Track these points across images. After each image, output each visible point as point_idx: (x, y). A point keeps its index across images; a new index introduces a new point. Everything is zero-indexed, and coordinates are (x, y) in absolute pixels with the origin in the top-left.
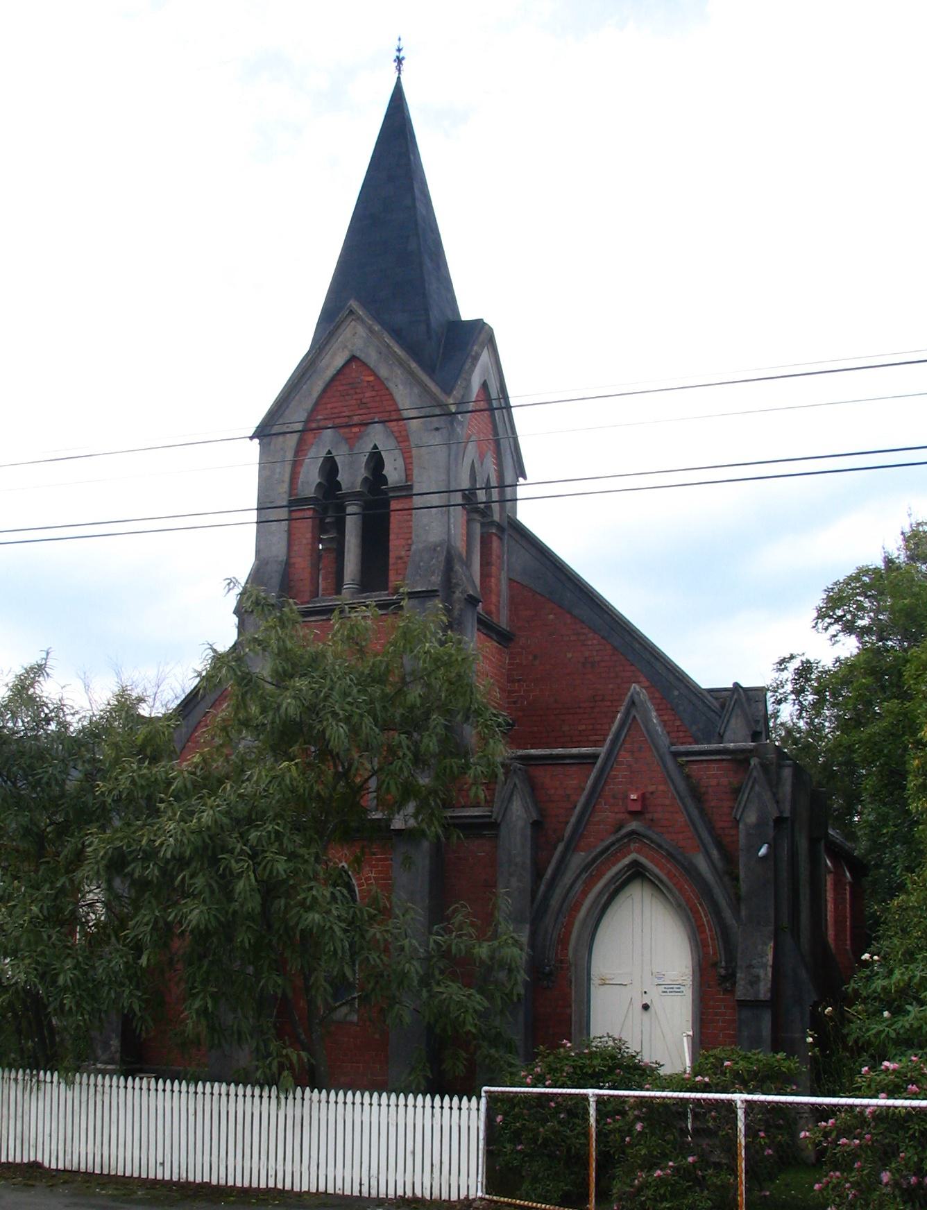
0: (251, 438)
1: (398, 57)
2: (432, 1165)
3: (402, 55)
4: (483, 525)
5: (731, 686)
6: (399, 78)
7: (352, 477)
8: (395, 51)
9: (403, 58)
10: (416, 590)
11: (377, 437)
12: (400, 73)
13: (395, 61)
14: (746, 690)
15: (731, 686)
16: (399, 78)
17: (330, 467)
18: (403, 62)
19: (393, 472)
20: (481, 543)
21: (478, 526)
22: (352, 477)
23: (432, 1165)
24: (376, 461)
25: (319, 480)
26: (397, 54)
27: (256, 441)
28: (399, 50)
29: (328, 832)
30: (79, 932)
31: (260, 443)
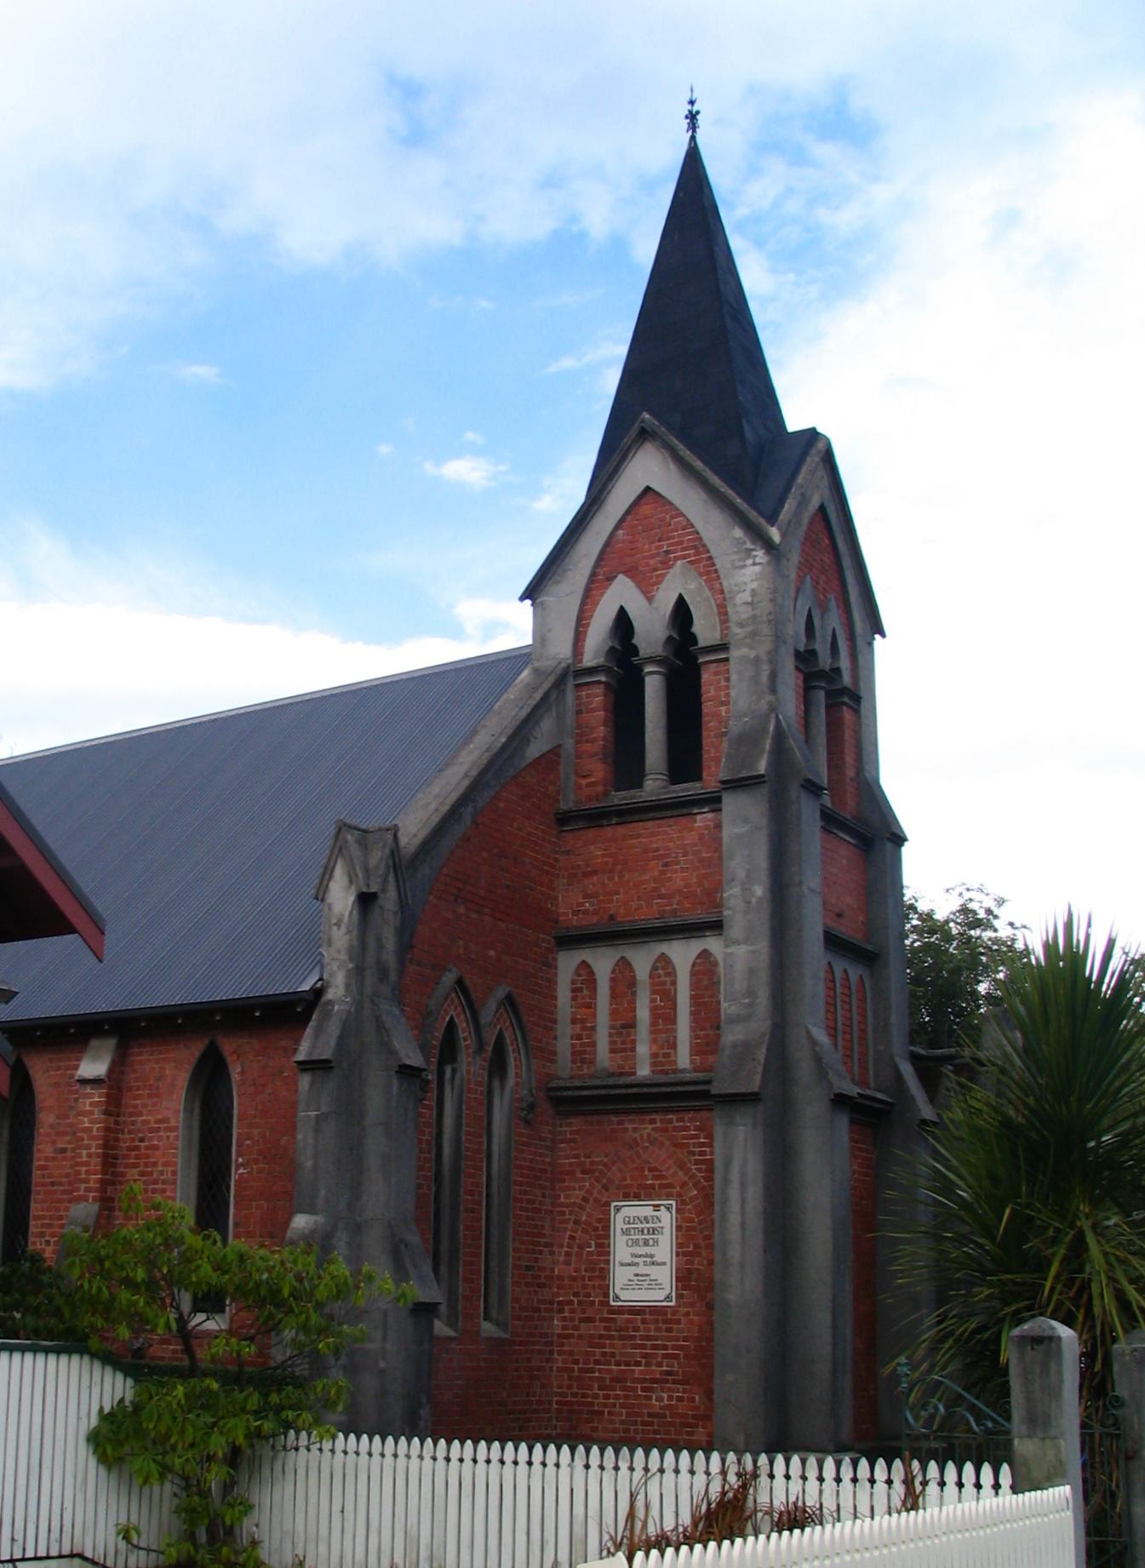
0: (522, 599)
1: (690, 112)
2: (49, 1531)
3: (695, 109)
4: (828, 694)
5: (794, 422)
6: (693, 138)
7: (651, 629)
8: (686, 104)
9: (698, 112)
10: (741, 776)
11: (677, 583)
12: (694, 131)
13: (687, 117)
14: (818, 433)
15: (794, 422)
16: (693, 138)
17: (623, 623)
18: (698, 117)
19: (705, 630)
20: (828, 725)
21: (822, 694)
22: (651, 629)
23: (49, 1531)
24: (682, 613)
25: (610, 644)
26: (690, 107)
27: (528, 602)
28: (692, 103)
29: (976, 1205)
30: (230, 1305)
31: (532, 605)
